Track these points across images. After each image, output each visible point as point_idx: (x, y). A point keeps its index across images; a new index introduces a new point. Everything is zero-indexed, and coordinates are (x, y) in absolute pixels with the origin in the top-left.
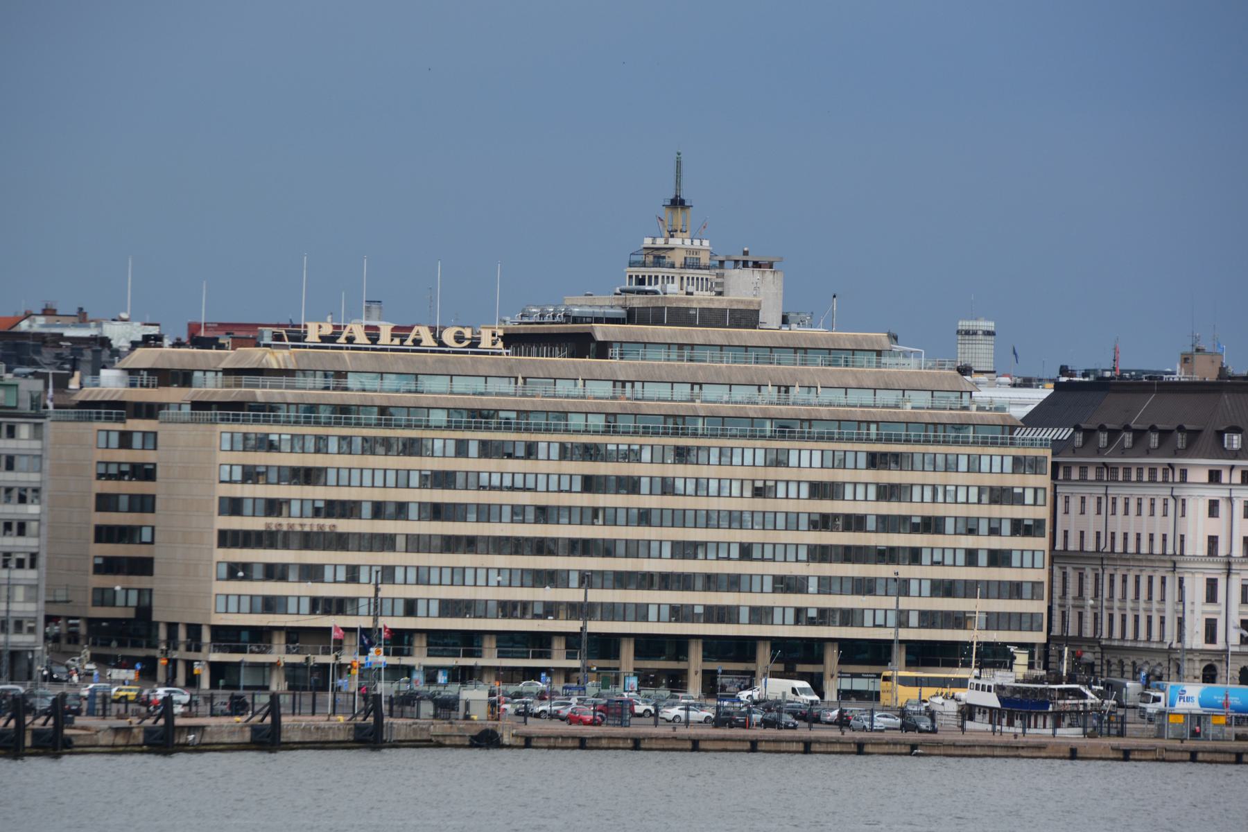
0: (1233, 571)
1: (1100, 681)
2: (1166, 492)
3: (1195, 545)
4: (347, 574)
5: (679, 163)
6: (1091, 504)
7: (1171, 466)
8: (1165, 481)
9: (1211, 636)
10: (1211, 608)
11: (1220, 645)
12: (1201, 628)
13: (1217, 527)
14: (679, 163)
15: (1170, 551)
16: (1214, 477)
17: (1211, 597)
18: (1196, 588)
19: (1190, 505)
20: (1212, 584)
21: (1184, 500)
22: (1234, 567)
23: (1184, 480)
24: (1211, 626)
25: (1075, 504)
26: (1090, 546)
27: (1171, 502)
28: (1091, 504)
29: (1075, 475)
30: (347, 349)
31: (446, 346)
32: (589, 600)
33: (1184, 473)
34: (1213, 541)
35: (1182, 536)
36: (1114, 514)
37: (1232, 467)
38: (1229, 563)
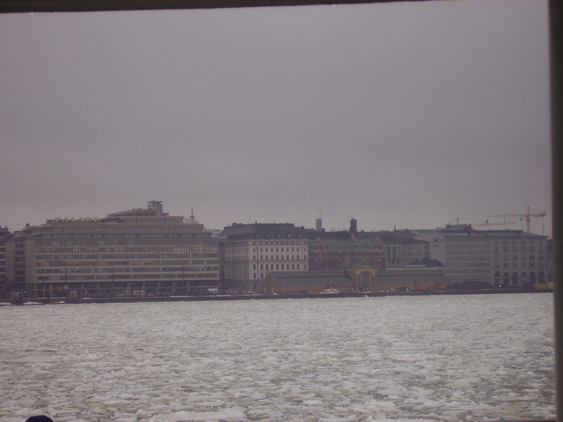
0: (553, 335)
1: (71, 247)
2: (244, 247)
3: (251, 258)
4: (173, 271)
5: (192, 209)
6: (231, 251)
7: (245, 242)
8: (244, 245)
9: (255, 277)
10: (254, 271)
11: (257, 278)
12: (252, 275)
13: (255, 254)
14: (192, 209)
15: (246, 260)
16: (254, 244)
17: (254, 268)
18: (251, 267)
19: (249, 249)
20: (254, 266)
21: (248, 249)
22: (259, 262)
23: (248, 244)
24: (255, 274)
25: (228, 251)
26: (231, 260)
27: (246, 249)
28: (231, 251)
29: (228, 246)
30: (79, 223)
31: (86, 222)
32: (183, 272)
33: (248, 243)
34: (254, 257)
35: (248, 256)
36: (235, 253)
37: (257, 241)
38: (258, 261)
